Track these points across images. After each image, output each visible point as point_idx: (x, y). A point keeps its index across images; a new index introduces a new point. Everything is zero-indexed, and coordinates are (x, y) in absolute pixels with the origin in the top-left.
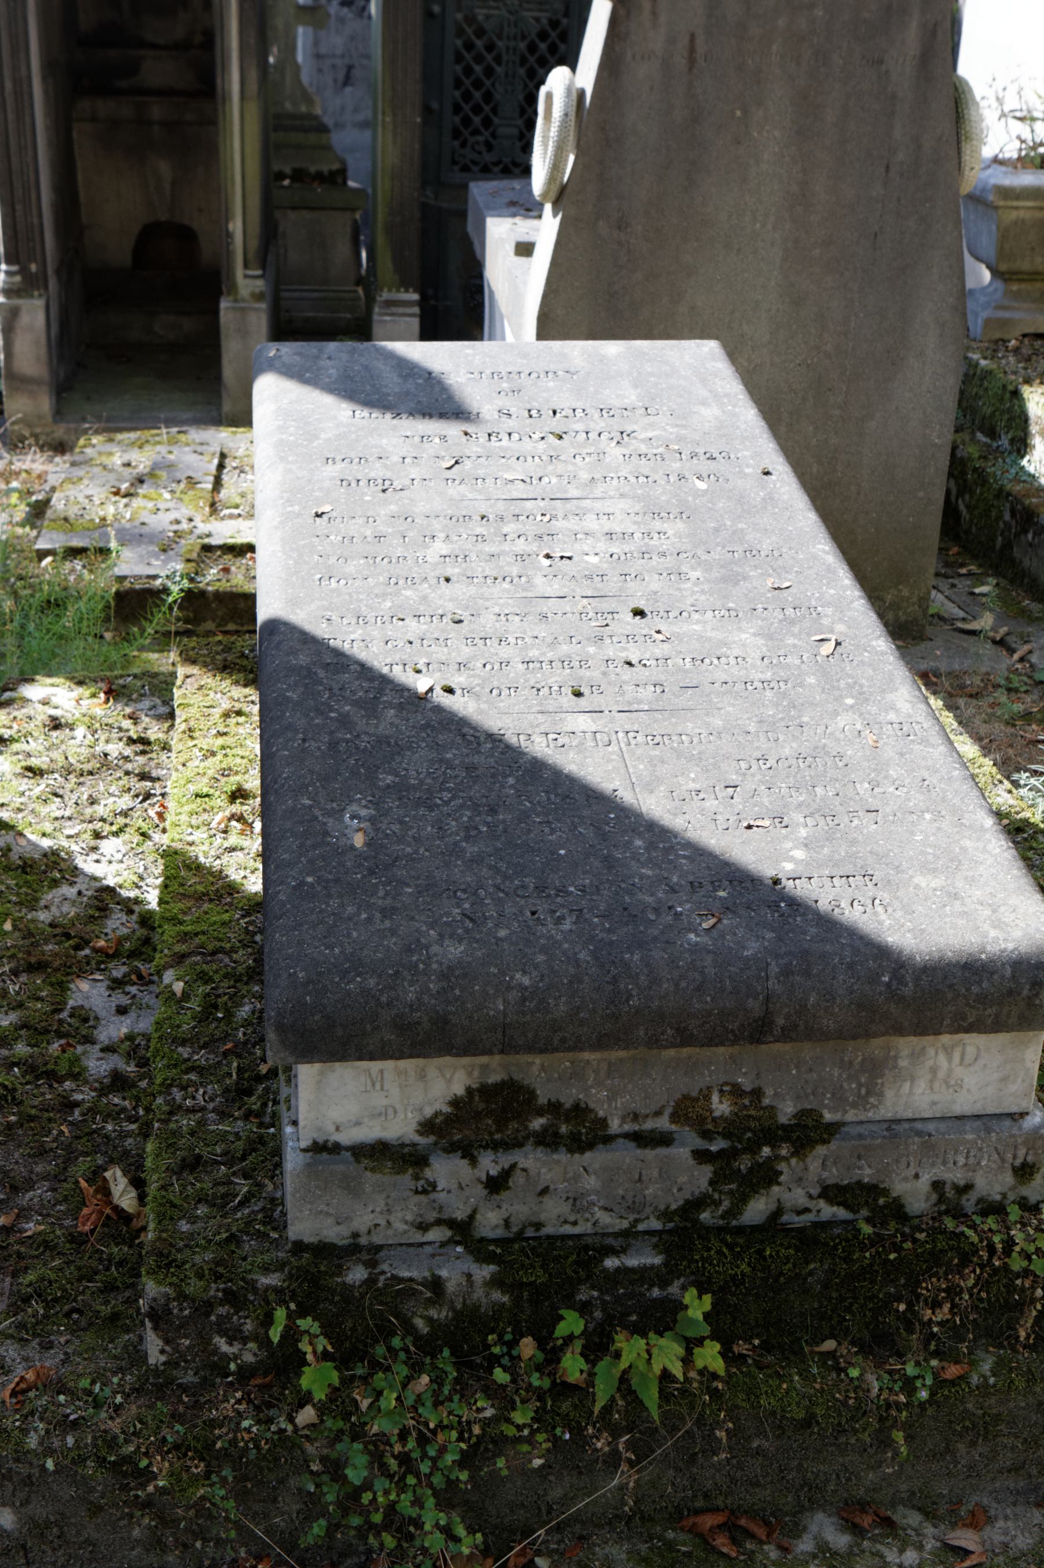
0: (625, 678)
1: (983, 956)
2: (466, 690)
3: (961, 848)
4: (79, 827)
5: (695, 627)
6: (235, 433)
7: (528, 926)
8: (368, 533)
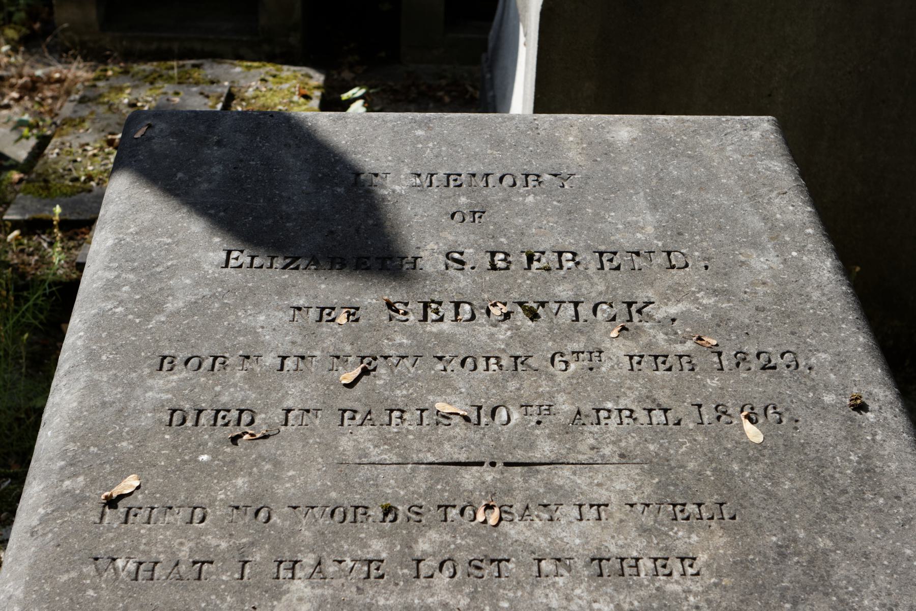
6: (249, 68)
8: (184, 554)
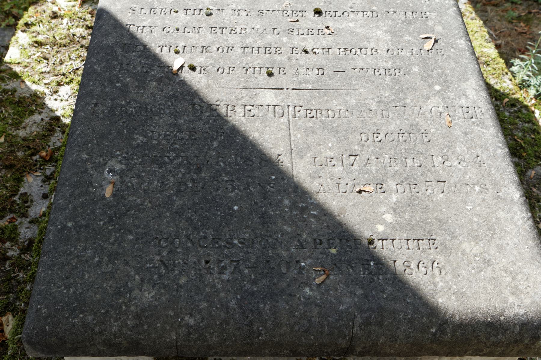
0: (301, 62)
1: (502, 318)
2: (203, 68)
3: (496, 219)
4: (51, 78)
5: (350, 24)
7: (201, 275)
